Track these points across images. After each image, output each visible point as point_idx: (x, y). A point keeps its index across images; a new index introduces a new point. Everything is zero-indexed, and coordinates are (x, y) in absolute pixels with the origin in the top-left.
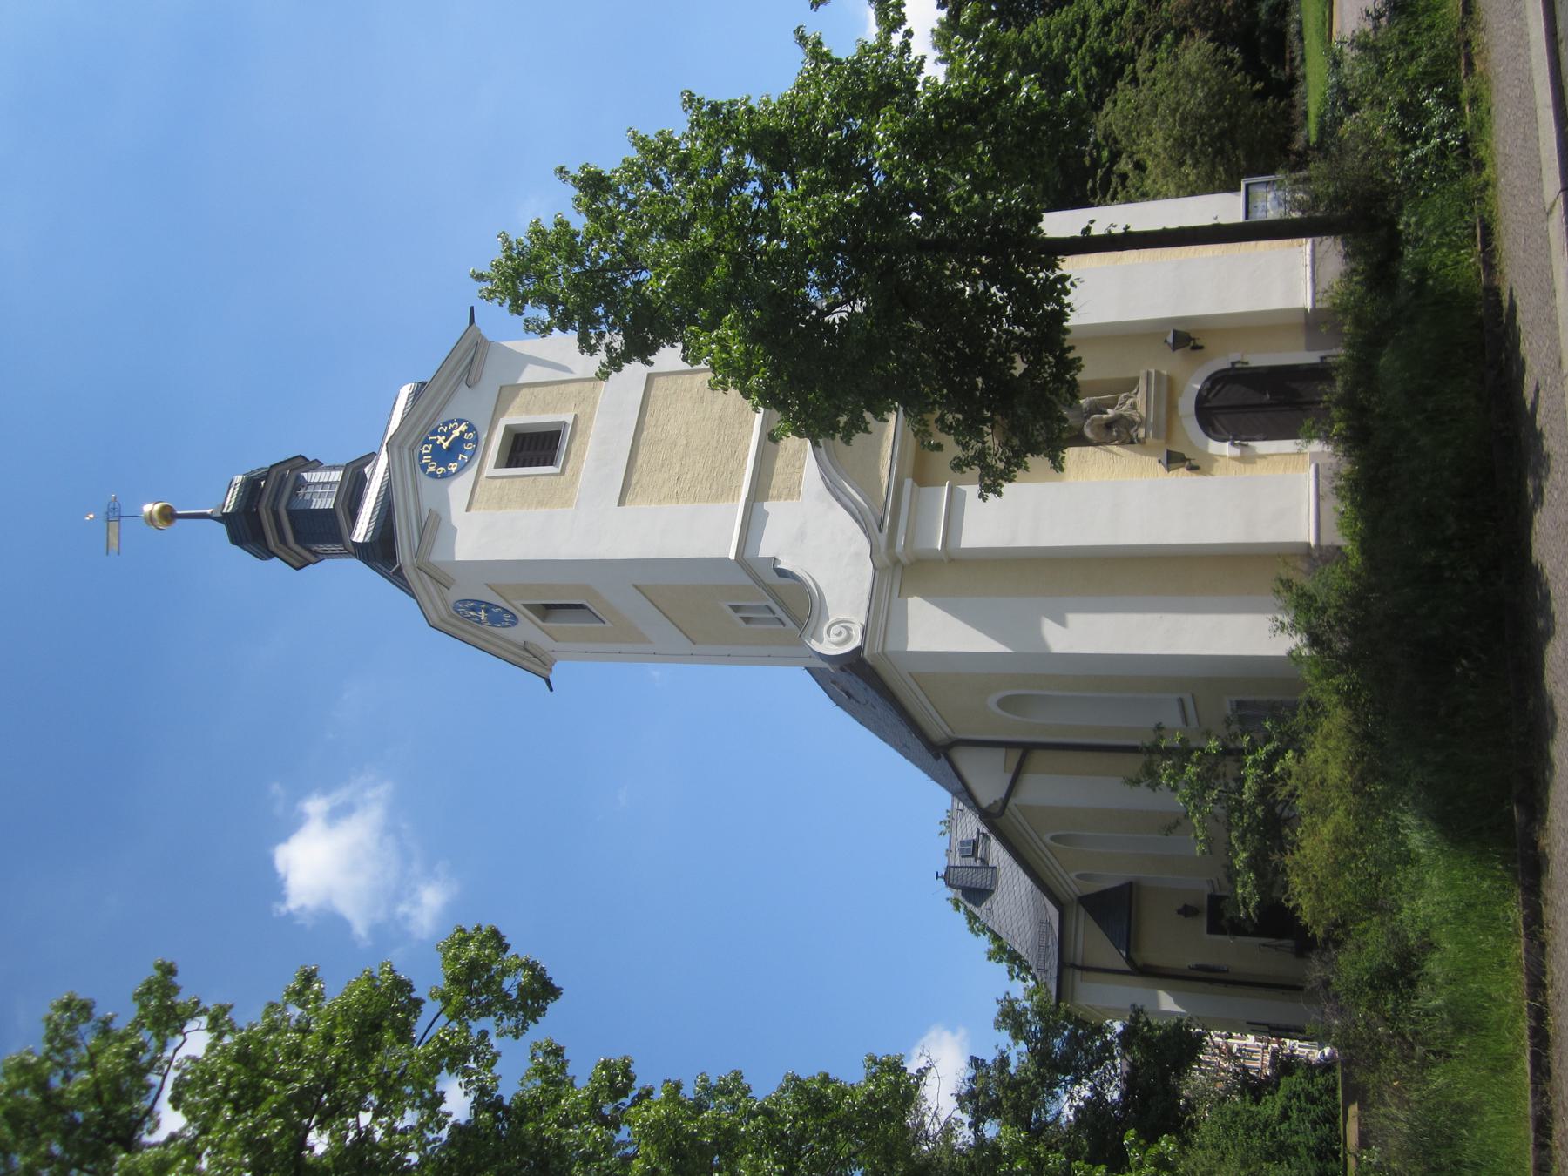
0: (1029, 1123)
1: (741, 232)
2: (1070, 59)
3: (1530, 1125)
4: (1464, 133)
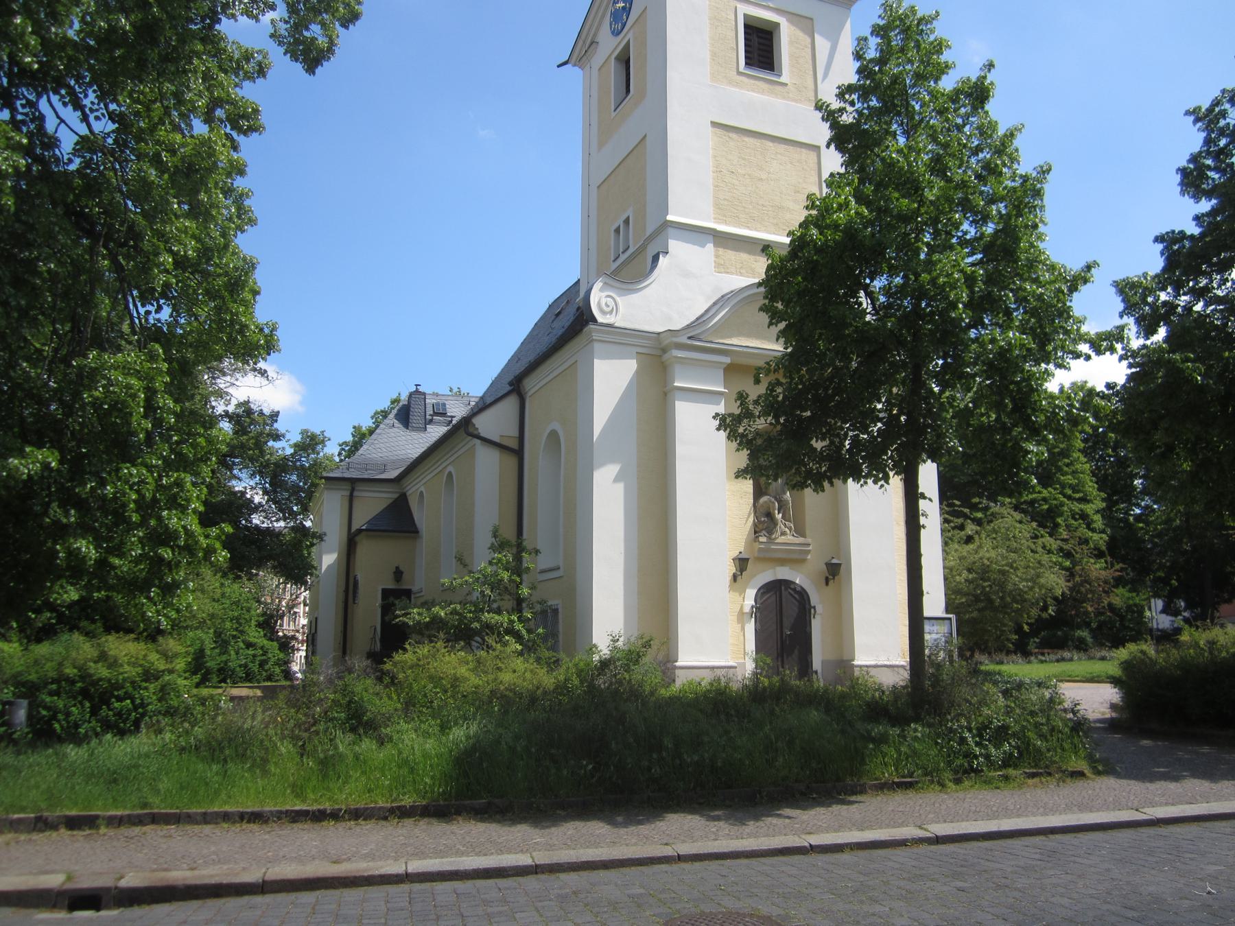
0: (231, 456)
1: (935, 221)
2: (1055, 489)
3: (256, 809)
4: (982, 771)
